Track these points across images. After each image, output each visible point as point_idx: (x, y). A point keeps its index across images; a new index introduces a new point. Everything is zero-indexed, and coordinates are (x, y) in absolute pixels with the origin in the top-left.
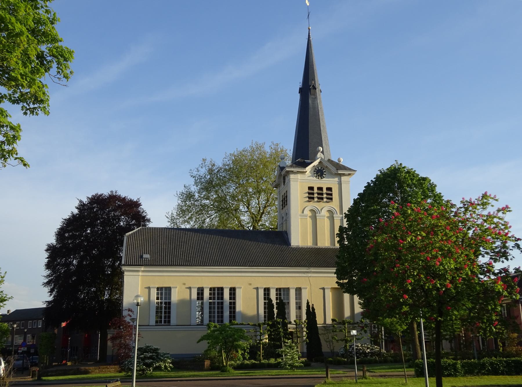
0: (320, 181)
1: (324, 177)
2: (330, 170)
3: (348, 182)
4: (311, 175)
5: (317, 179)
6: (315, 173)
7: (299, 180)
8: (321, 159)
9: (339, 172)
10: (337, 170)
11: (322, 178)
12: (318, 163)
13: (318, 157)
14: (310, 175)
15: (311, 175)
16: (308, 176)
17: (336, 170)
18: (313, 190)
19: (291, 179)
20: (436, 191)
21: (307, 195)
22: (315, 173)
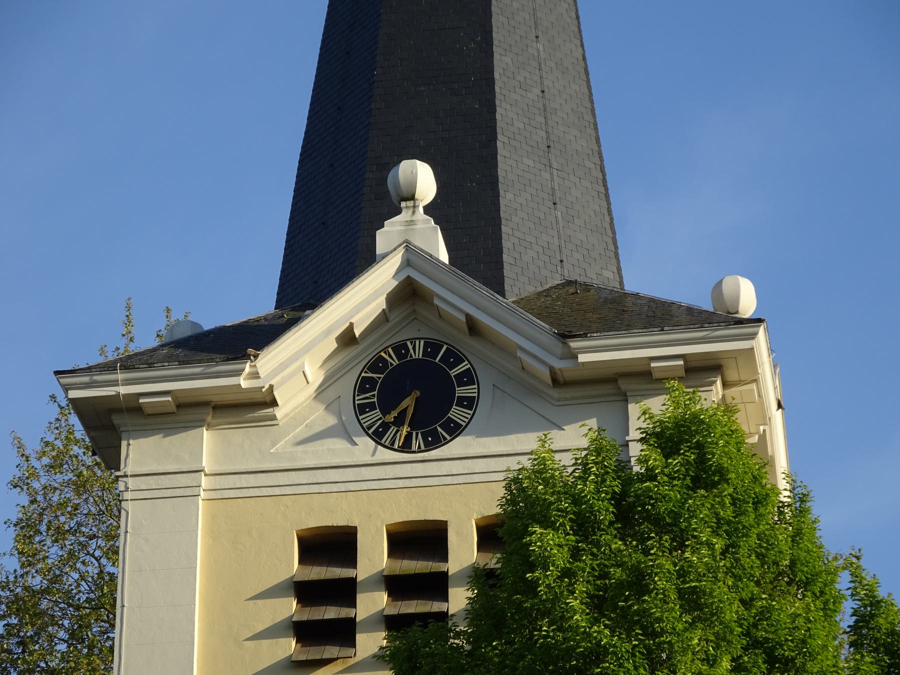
0: (419, 469)
1: (455, 430)
2: (506, 349)
3: (189, 492)
4: (332, 421)
5: (385, 454)
6: (373, 397)
7: (204, 481)
8: (407, 263)
9: (583, 358)
10: (564, 336)
11: (432, 442)
12: (380, 304)
13: (379, 250)
14: (323, 419)
15: (332, 421)
16: (300, 432)
17: (556, 346)
18: (442, 553)
19: (131, 482)
20: (833, 552)
21: (290, 607)
22: (373, 397)
